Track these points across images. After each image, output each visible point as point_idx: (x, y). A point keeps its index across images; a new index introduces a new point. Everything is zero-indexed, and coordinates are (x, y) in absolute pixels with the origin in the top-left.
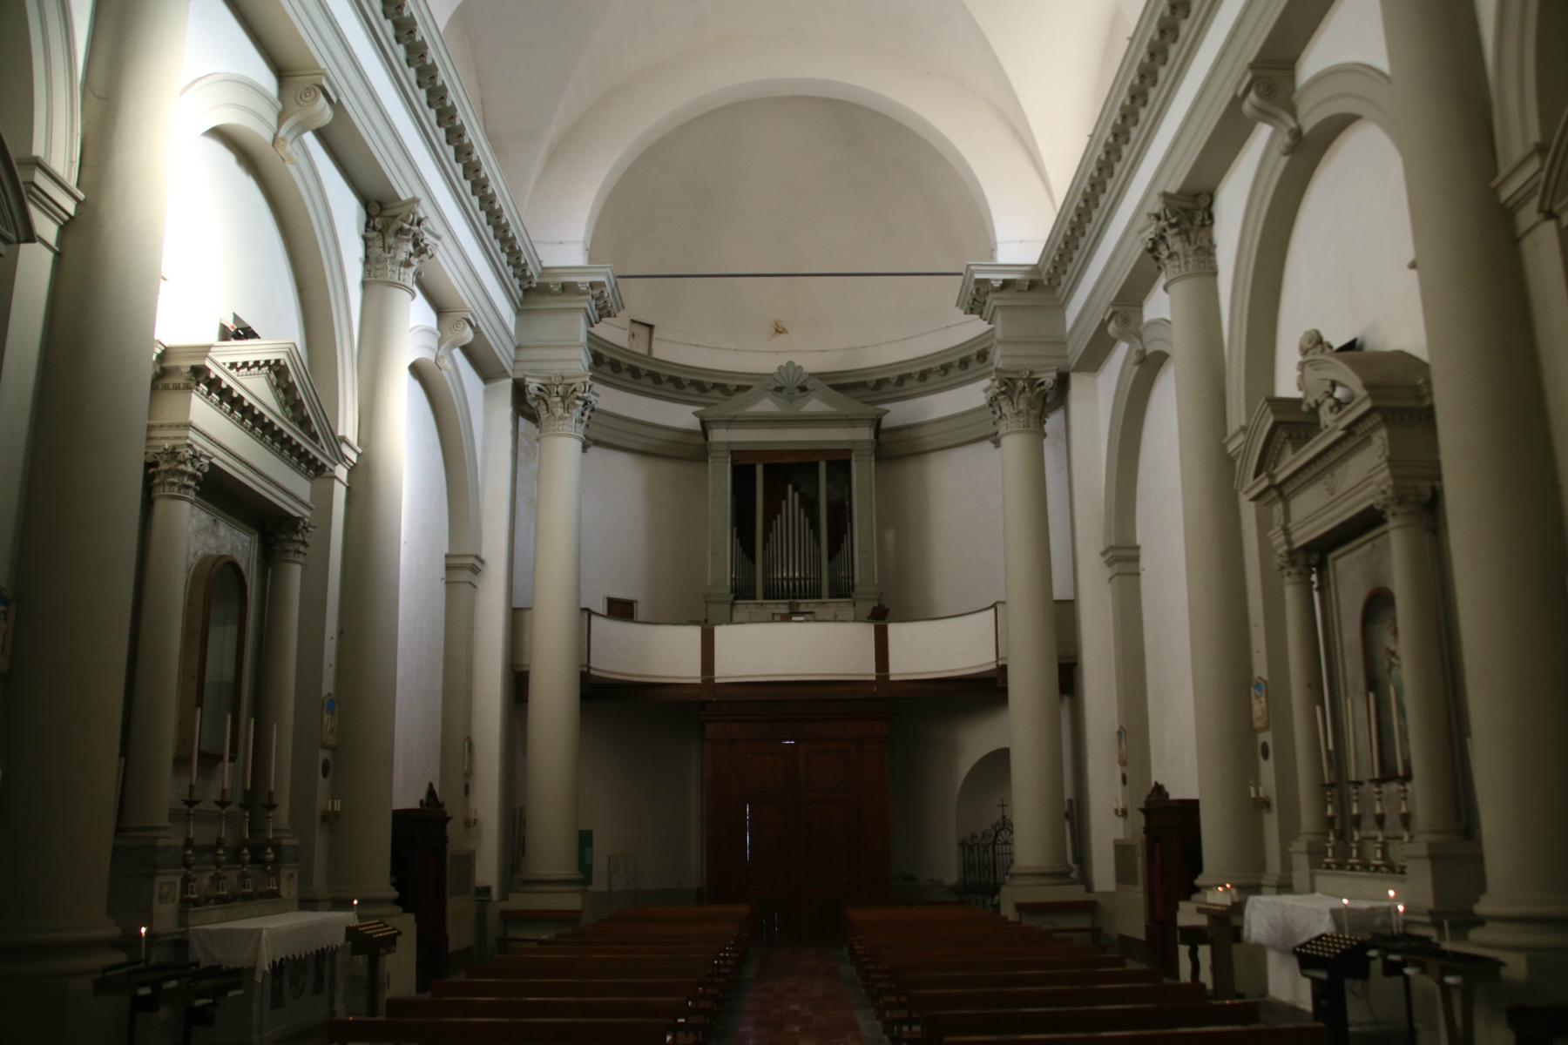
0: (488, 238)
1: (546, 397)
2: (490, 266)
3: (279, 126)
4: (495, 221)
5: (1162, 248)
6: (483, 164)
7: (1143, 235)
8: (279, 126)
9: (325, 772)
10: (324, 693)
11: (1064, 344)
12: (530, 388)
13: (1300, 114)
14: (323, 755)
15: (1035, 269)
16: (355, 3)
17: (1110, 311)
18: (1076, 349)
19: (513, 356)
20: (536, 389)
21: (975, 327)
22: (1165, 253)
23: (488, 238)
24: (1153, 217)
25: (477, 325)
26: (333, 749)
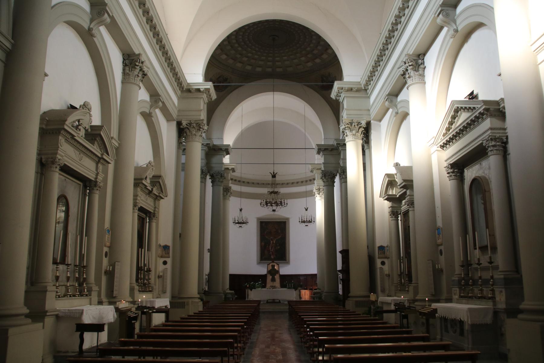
1: (189, 128)
2: (161, 67)
3: (91, 23)
5: (407, 73)
6: (172, 57)
7: (400, 69)
8: (91, 23)
9: (106, 256)
10: (106, 227)
11: (369, 110)
13: (458, 23)
16: (128, 1)
17: (440, 9)
18: (374, 112)
19: (177, 114)
24: (403, 62)
25: (113, 16)
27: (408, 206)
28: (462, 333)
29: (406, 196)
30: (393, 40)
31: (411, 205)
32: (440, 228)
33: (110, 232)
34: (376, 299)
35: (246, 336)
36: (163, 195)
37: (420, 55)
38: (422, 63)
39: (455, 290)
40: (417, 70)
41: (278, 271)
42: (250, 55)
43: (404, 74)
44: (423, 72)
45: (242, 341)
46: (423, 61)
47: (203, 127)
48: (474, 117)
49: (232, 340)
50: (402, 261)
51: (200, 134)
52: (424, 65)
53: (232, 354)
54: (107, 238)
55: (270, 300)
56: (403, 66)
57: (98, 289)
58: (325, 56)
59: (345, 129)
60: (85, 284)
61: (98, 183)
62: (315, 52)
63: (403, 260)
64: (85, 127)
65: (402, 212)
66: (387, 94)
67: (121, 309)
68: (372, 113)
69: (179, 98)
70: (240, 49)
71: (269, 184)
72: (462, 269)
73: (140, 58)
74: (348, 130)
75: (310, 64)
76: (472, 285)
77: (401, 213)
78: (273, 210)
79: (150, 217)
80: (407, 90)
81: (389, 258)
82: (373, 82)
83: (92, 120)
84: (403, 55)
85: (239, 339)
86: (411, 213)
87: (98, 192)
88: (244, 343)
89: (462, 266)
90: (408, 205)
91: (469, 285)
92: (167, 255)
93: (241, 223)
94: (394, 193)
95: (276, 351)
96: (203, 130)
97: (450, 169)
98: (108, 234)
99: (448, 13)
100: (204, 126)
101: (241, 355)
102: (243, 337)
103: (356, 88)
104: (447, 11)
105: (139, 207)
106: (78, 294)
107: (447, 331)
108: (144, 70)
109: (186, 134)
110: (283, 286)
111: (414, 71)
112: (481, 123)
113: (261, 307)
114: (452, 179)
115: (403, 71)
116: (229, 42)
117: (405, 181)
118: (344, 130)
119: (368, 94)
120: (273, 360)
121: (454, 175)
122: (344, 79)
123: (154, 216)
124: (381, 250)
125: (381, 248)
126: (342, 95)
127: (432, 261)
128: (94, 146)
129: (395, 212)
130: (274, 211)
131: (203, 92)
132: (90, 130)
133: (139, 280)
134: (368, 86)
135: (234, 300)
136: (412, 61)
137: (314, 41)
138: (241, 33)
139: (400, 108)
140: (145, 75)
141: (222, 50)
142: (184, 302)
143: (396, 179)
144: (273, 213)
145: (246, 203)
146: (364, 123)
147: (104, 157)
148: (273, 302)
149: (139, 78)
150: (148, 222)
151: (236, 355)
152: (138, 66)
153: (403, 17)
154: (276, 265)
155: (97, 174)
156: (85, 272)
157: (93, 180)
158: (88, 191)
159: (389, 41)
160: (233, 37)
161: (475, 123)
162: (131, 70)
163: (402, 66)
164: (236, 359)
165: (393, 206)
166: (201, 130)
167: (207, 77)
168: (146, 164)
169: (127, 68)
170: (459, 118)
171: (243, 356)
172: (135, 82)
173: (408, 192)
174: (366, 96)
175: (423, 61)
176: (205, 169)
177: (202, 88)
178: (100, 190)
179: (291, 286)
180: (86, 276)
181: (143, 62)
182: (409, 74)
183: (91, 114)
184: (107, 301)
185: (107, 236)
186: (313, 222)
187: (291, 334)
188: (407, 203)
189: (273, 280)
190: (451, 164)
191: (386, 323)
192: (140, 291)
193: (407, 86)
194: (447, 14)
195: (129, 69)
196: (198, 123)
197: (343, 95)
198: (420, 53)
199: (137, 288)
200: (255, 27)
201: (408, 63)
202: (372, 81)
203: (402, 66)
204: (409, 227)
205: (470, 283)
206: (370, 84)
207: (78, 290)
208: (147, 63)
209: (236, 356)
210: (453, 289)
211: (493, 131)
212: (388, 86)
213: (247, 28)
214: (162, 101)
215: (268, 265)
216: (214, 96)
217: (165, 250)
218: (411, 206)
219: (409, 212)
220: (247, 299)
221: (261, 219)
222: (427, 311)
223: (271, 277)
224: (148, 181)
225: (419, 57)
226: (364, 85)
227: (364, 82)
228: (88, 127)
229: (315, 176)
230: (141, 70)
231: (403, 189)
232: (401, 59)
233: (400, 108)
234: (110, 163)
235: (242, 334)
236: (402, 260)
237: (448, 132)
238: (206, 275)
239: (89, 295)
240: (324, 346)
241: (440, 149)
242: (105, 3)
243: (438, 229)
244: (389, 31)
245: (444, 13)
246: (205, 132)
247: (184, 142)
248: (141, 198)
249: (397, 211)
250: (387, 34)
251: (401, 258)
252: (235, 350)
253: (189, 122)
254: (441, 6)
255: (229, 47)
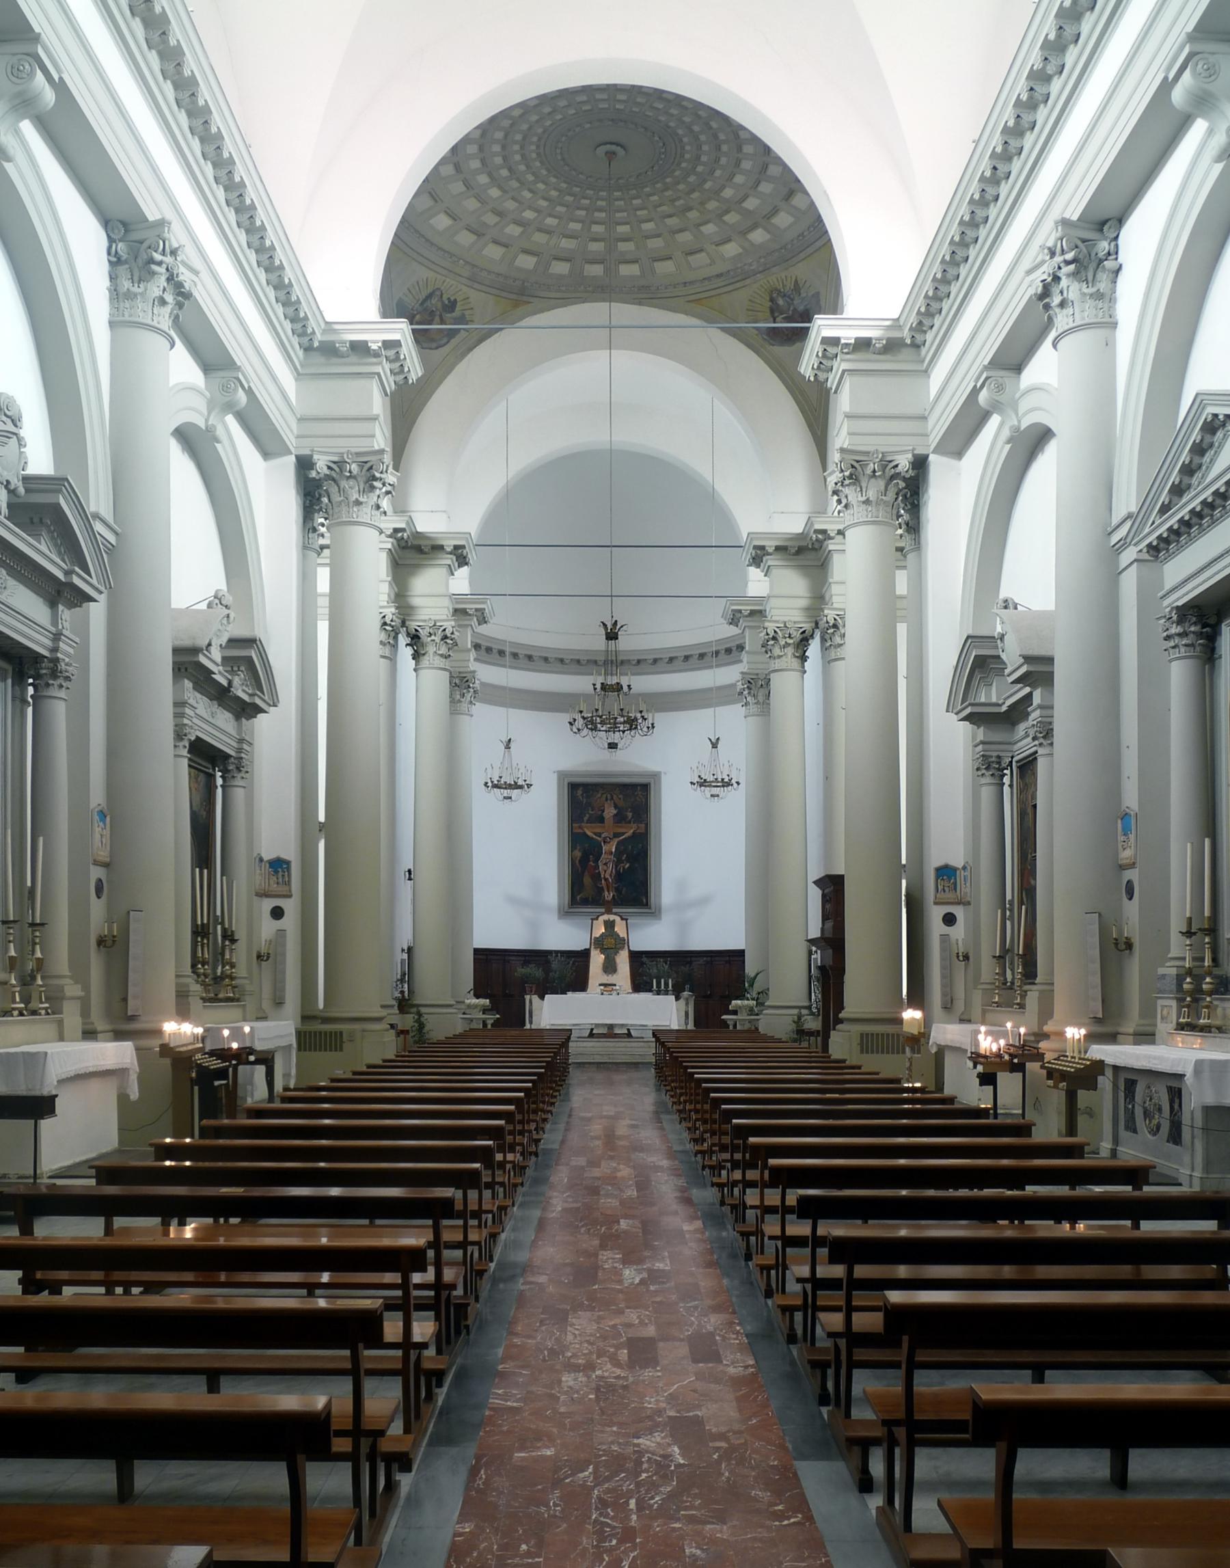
0: (277, 318)
4: (237, 201)
5: (1055, 290)
12: (318, 465)
14: (96, 873)
15: (896, 324)
18: (938, 426)
19: (295, 432)
20: (325, 468)
21: (733, 631)
22: (1056, 300)
23: (240, 246)
24: (1046, 251)
25: (61, 79)
26: (106, 865)
27: (1036, 742)
28: (1175, 1137)
29: (1029, 709)
30: (1016, 165)
31: (1044, 737)
32: (1132, 813)
33: (108, 819)
34: (922, 1031)
35: (530, 1131)
36: (264, 701)
37: (1104, 223)
38: (1109, 254)
39: (1166, 1006)
40: (1090, 278)
41: (623, 939)
42: (529, 215)
43: (1046, 293)
44: (1110, 285)
45: (519, 1144)
46: (1113, 244)
47: (382, 476)
48: (1201, 502)
49: (491, 1143)
50: (1008, 913)
51: (375, 499)
52: (1116, 259)
53: (488, 1183)
54: (97, 836)
55: (597, 1025)
56: (1046, 265)
57: (83, 994)
58: (783, 220)
59: (843, 483)
60: (39, 977)
61: (63, 664)
62: (751, 204)
63: (1011, 910)
64: (8, 482)
65: (1014, 759)
66: (986, 362)
67: (178, 1050)
68: (934, 427)
69: (299, 374)
70: (495, 193)
71: (595, 662)
72: (1188, 942)
73: (166, 235)
74: (852, 488)
75: (731, 249)
76: (1211, 993)
77: (1011, 762)
78: (609, 744)
79: (225, 772)
80: (1054, 350)
81: (969, 903)
82: (941, 318)
83: (26, 458)
84: (1049, 224)
85: (509, 1138)
86: (1041, 765)
87: (62, 694)
88: (522, 1154)
89: (1189, 934)
90: (1034, 739)
91: (1201, 991)
92: (282, 889)
93: (509, 787)
94: (994, 700)
95: (619, 1174)
96: (384, 485)
97: (1174, 625)
98: (101, 824)
99: (1002, 385)
100: (386, 472)
101: (515, 1185)
102: (521, 1133)
103: (884, 342)
104: (1212, 59)
105: (193, 739)
106: (46, 1009)
107: (1132, 1127)
108: (181, 278)
109: (329, 501)
110: (640, 984)
111: (1080, 281)
112: (1196, 538)
113: (573, 1047)
114: (1178, 655)
115: (1042, 281)
116: (457, 167)
117: (1028, 659)
118: (839, 487)
119: (923, 361)
120: (610, 1200)
121: (1186, 645)
122: (845, 309)
123: (239, 769)
124: (945, 878)
125: (946, 873)
126: (836, 364)
127: (1100, 915)
128: (40, 544)
129: (993, 759)
130: (613, 746)
131: (376, 354)
132: (22, 490)
133: (200, 966)
134: (925, 332)
135: (489, 1027)
136: (1077, 247)
137: (746, 165)
138: (499, 135)
139: (1025, 414)
140: (183, 295)
141: (433, 196)
142: (341, 1033)
143: (1001, 653)
144: (607, 754)
145: (520, 721)
146: (904, 463)
147: (76, 581)
148: (610, 1032)
149: (168, 309)
150: (221, 786)
151: (502, 1184)
152: (160, 264)
153: (1055, 78)
154: (617, 919)
155: (57, 637)
156: (37, 940)
157: (46, 657)
158: (31, 690)
159: (1002, 168)
160: (472, 149)
161: (1204, 521)
162: (136, 278)
163: (1043, 262)
164: (501, 1195)
165: (987, 740)
166: (377, 484)
167: (392, 306)
168: (207, 601)
169: (122, 270)
170: (1216, 452)
171: (519, 1189)
172: (155, 321)
173: (1037, 698)
174: (920, 368)
175: (1113, 244)
176: (393, 614)
177: (375, 339)
178: (68, 688)
179: (666, 985)
180: (42, 953)
181: (177, 249)
182: (1062, 292)
183: (23, 438)
184: (108, 1027)
185: (97, 830)
186: (735, 785)
187: (662, 1129)
188: (1032, 733)
189: (610, 968)
190: (1177, 607)
191: (951, 1100)
192: (204, 1000)
193: (1053, 335)
194: (1209, 69)
195: (132, 275)
196: (366, 462)
197: (840, 365)
198: (1107, 217)
199: (196, 988)
200: (547, 110)
201: (1063, 252)
202: (938, 315)
203: (1043, 262)
204: (1035, 806)
205: (1204, 986)
206: (932, 327)
207: (19, 995)
208: (189, 254)
209: (501, 1190)
210: (1160, 1002)
211: (987, 747)
212: (1180, 13)
213: (517, 113)
214: (246, 386)
215: (592, 919)
216: (415, 371)
217: (276, 872)
218: (1045, 743)
219: (1036, 758)
220: (528, 1026)
221: (572, 775)
222: (1072, 1067)
223: (603, 956)
224: (216, 654)
225: (1101, 230)
226: (911, 329)
227: (913, 319)
228: (16, 483)
229: (744, 637)
230: (173, 279)
231: (1021, 685)
232: (1039, 240)
233: (1025, 414)
234: (95, 601)
235: (519, 1127)
236: (1010, 910)
237: (1175, 499)
238: (403, 950)
239: (55, 1009)
240: (765, 1166)
241: (1147, 557)
242: (32, 29)
243: (1125, 816)
244: (1006, 130)
245: (1200, 66)
246: (388, 493)
247: (323, 525)
248: (197, 711)
249: (999, 757)
250: (1009, 117)
251: (1008, 906)
252: (487, 1194)
253: (336, 459)
254: (1191, 38)
255: (458, 187)
